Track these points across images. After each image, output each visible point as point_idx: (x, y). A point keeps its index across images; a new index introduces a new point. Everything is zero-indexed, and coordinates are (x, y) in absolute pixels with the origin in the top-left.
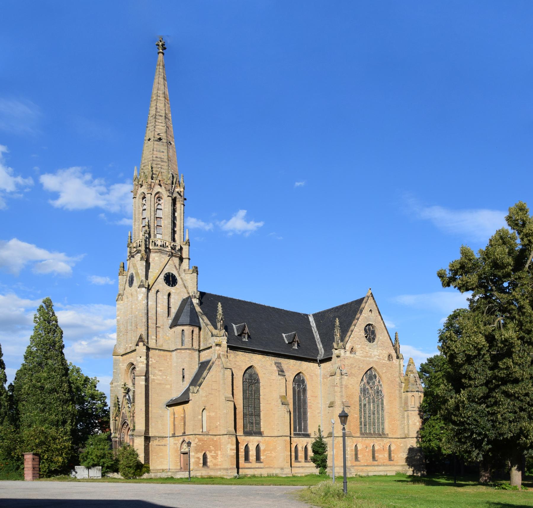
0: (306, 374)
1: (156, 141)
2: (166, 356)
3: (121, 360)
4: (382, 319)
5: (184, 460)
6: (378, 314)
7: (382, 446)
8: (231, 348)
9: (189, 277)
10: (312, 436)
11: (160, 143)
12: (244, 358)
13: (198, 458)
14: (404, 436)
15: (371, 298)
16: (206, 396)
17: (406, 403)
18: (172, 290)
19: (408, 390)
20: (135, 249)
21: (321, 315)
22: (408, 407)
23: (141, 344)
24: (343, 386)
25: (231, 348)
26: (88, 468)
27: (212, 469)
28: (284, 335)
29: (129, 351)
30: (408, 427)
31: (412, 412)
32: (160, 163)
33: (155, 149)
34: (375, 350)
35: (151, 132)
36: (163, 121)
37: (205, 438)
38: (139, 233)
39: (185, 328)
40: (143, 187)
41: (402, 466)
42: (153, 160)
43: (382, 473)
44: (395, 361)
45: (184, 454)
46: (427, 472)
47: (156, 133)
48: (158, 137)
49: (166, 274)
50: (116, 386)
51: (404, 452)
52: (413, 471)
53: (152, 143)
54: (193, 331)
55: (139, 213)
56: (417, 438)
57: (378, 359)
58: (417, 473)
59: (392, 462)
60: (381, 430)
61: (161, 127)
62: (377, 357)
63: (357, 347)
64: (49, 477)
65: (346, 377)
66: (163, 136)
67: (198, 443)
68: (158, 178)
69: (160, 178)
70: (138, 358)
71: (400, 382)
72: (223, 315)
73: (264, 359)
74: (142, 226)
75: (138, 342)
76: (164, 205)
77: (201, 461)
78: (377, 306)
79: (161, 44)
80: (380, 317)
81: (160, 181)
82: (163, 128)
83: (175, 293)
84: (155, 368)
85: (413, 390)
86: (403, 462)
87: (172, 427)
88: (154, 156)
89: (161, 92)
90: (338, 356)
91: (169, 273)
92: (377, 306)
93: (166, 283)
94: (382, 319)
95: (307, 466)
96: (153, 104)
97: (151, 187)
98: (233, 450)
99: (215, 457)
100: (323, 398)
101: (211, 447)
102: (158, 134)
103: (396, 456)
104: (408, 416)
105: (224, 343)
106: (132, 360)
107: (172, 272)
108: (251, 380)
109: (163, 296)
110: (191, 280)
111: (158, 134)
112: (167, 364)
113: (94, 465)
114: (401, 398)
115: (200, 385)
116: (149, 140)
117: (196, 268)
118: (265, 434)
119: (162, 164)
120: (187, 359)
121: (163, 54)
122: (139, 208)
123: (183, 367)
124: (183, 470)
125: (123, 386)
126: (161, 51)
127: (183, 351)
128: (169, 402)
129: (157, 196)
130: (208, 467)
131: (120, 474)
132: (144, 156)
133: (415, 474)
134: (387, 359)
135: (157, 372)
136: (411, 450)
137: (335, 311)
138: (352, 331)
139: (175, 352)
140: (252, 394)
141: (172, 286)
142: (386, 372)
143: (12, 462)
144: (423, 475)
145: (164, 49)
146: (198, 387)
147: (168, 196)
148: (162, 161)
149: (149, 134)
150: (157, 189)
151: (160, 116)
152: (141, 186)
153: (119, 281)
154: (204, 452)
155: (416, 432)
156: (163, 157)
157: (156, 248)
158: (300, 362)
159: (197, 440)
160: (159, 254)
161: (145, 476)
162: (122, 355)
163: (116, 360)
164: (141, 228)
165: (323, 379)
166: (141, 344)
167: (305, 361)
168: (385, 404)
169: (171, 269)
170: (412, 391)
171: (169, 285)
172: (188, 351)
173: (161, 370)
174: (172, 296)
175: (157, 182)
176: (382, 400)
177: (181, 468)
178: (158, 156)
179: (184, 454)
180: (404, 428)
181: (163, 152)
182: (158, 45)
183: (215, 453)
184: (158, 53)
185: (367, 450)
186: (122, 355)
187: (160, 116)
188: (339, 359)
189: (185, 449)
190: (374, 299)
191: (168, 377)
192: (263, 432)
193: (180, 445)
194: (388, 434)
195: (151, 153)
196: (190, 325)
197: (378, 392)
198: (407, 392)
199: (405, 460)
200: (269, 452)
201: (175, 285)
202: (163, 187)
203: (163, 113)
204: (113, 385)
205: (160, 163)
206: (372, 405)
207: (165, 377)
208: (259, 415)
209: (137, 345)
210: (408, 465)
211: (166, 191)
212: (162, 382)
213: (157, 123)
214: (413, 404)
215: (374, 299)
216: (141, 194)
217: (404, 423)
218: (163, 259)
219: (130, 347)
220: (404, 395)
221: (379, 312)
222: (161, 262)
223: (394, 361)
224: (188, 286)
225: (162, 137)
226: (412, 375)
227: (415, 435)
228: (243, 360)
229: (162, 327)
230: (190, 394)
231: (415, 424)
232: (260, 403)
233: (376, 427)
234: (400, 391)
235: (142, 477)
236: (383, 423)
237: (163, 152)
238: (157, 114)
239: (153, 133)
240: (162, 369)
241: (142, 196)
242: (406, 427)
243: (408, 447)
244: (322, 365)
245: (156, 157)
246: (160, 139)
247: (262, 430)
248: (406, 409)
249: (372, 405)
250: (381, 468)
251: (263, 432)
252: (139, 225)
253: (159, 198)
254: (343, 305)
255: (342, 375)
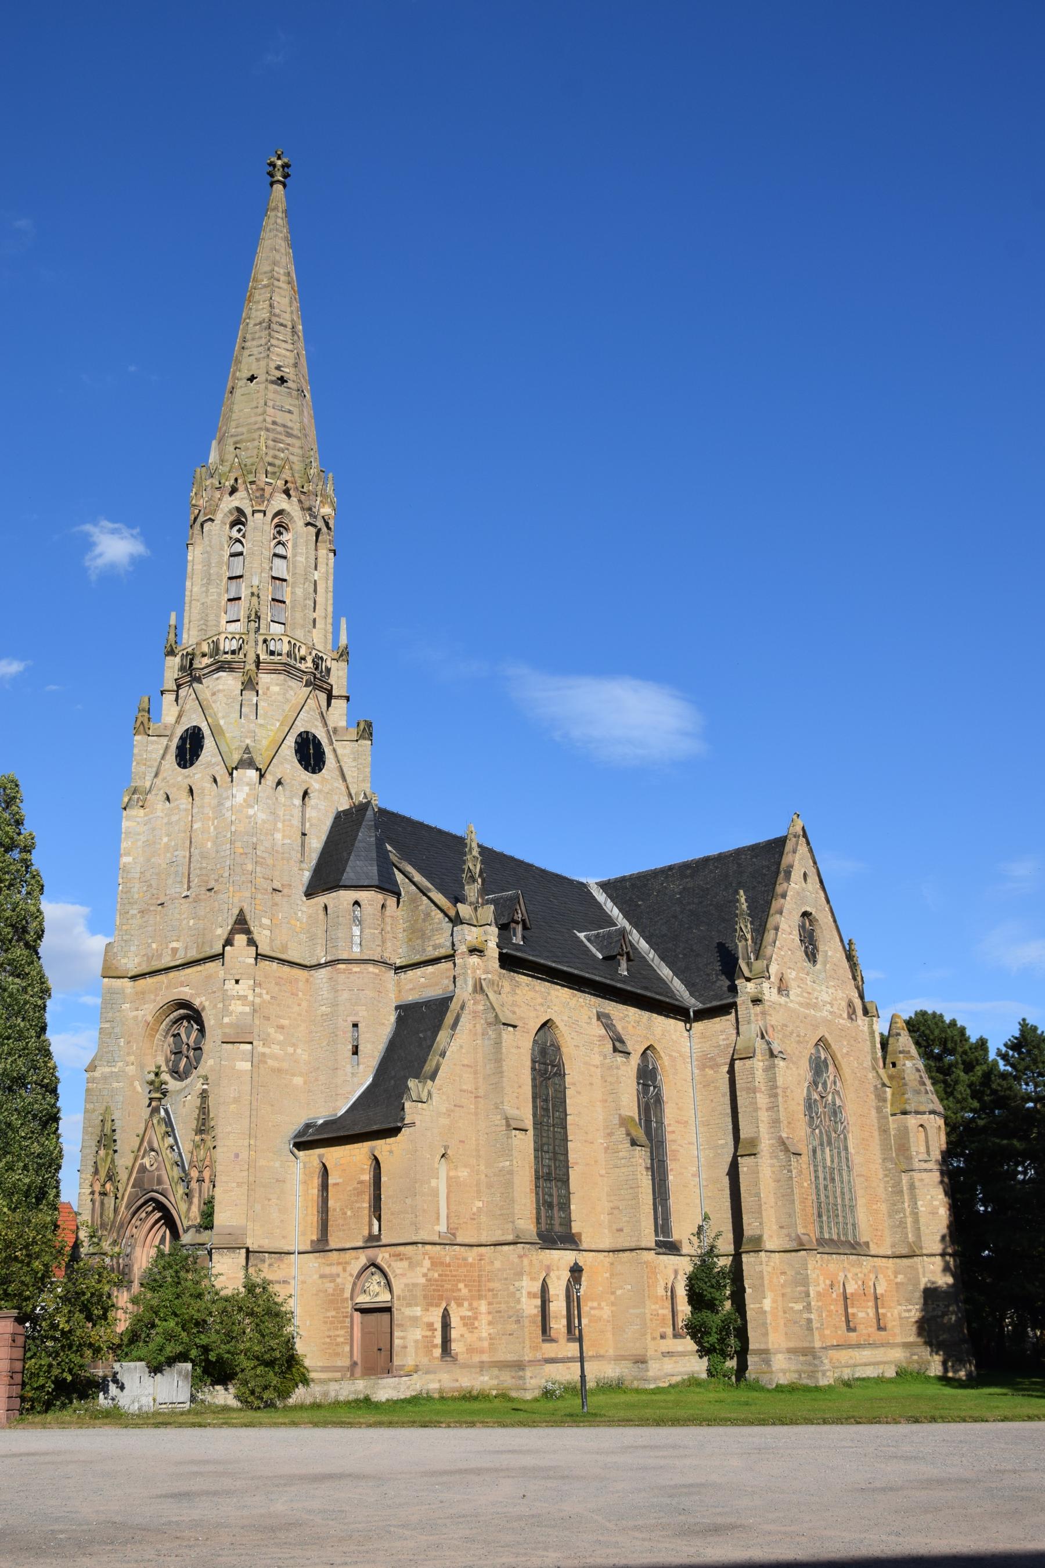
0: (662, 1054)
1: (272, 382)
2: (297, 980)
3: (128, 991)
4: (828, 902)
5: (364, 1333)
6: (818, 885)
7: (860, 1283)
8: (509, 962)
9: (347, 751)
10: (686, 1249)
11: (282, 389)
12: (531, 994)
13: (430, 1326)
14: (905, 1251)
15: (802, 840)
16: (449, 1113)
17: (903, 1148)
18: (314, 781)
19: (908, 1108)
20: (206, 661)
21: (633, 885)
22: (909, 1158)
23: (240, 939)
24: (779, 1091)
25: (509, 962)
26: (156, 1369)
27: (465, 1366)
28: (582, 935)
29: (167, 961)
30: (916, 1221)
31: (924, 1175)
32: (283, 438)
33: (270, 403)
34: (824, 988)
35: (258, 360)
36: (289, 338)
37: (447, 1254)
38: (218, 616)
39: (362, 896)
40: (237, 495)
41: (906, 1345)
42: (267, 430)
43: (871, 1372)
44: (862, 1021)
45: (364, 1311)
46: (976, 1367)
47: (272, 365)
48: (278, 374)
49: (300, 735)
50: (105, 1078)
51: (909, 1301)
52: (944, 1363)
53: (263, 386)
54: (383, 906)
55: (220, 564)
56: (943, 1255)
57: (831, 1012)
58: (955, 1371)
59: (883, 1333)
60: (850, 1232)
61: (284, 352)
62: (828, 1007)
63: (791, 975)
64: (48, 1406)
65: (782, 1063)
66: (288, 372)
67: (430, 1275)
68: (283, 476)
69: (287, 475)
70: (230, 984)
71: (878, 1083)
72: (482, 862)
73: (573, 1003)
74: (226, 597)
75: (232, 932)
76: (295, 546)
77: (438, 1340)
78: (815, 863)
79: (279, 163)
80: (822, 895)
81: (286, 482)
82: (288, 354)
83: (320, 791)
84: (268, 1019)
85: (922, 1109)
86: (911, 1336)
87: (314, 1219)
88: (269, 419)
89: (282, 271)
90: (756, 1001)
91: (307, 733)
92: (815, 863)
93: (300, 761)
94: (828, 902)
95: (680, 1349)
96: (260, 296)
97: (261, 496)
98: (535, 1296)
99: (469, 1323)
100: (701, 1129)
101: (461, 1286)
102: (278, 368)
103: (889, 1315)
104: (912, 1187)
105: (492, 949)
106: (185, 993)
107: (313, 731)
108: (548, 1068)
109: (291, 798)
110: (355, 760)
111: (278, 368)
112: (296, 1009)
113: (171, 1361)
114: (884, 1131)
115: (433, 1077)
116: (252, 379)
117: (369, 725)
118: (584, 1245)
119: (289, 440)
120: (369, 993)
121: (285, 186)
122: (222, 549)
123: (355, 1019)
124: (358, 1370)
125: (152, 1076)
126: (281, 179)
127: (356, 968)
128: (299, 1135)
129: (276, 520)
130: (455, 1359)
131: (232, 1390)
132: (234, 416)
133: (950, 1374)
134: (845, 1015)
135: (271, 1031)
136: (930, 1294)
137: (683, 876)
138: (777, 929)
139: (323, 972)
140: (547, 1110)
141: (314, 772)
142: (847, 1054)
143: (105, 1338)
144: (969, 1375)
145: (286, 176)
146: (429, 1082)
147: (308, 524)
148: (289, 435)
149: (248, 365)
150: (280, 502)
151: (281, 325)
152: (233, 490)
153: (136, 751)
154: (444, 1305)
155: (939, 1238)
156: (290, 424)
157: (276, 658)
158: (646, 1015)
159: (427, 1263)
160: (282, 677)
161: (300, 1395)
162: (134, 978)
163: (111, 992)
164: (223, 603)
165: (703, 1067)
166: (240, 939)
167: (660, 1013)
168: (851, 1150)
169: (309, 723)
170: (917, 1113)
171: (306, 769)
172: (371, 968)
173: (282, 1027)
174: (312, 801)
175: (280, 483)
176: (845, 1138)
177: (355, 1364)
178: (279, 420)
179: (364, 1311)
180: (902, 1224)
181: (290, 412)
182: (273, 165)
183: (471, 1308)
184: (272, 184)
185: (834, 1295)
186: (134, 978)
187: (281, 325)
188: (758, 1009)
189: (375, 1293)
190: (808, 843)
191: (299, 1051)
192: (580, 1234)
193: (352, 1280)
194: (867, 1244)
195: (260, 410)
196: (381, 888)
197: (835, 1113)
198: (904, 1113)
199: (914, 1329)
200: (595, 1304)
201: (320, 770)
202: (294, 499)
203: (286, 318)
204: (97, 1074)
205: (283, 438)
206: (827, 1150)
207: (290, 1050)
208: (565, 1181)
209: (229, 942)
210: (928, 1343)
211: (303, 509)
212: (285, 1065)
213: (273, 342)
214: (923, 1149)
215: (808, 843)
216: (230, 512)
217: (903, 1210)
218: (292, 693)
219: (175, 951)
220: (893, 1123)
221: (821, 882)
222: (288, 700)
223: (859, 1022)
224: (353, 774)
225: (286, 377)
226: (909, 1064)
227: (938, 1248)
228: (536, 1000)
229: (285, 891)
230: (408, 1105)
231: (934, 1213)
232: (565, 1140)
233: (841, 1219)
234: (879, 1110)
235: (291, 1401)
236: (852, 1208)
237: (290, 412)
238: (275, 319)
239: (263, 363)
240: (285, 1022)
241: (232, 518)
242: (909, 1220)
243: (922, 1287)
244: (698, 1026)
245: (274, 423)
246: (282, 380)
247: (575, 1228)
248: (904, 1167)
249: (827, 1150)
250: (866, 1354)
251: (580, 1234)
252: (219, 595)
253: (281, 528)
254: (706, 860)
255: (772, 1055)
